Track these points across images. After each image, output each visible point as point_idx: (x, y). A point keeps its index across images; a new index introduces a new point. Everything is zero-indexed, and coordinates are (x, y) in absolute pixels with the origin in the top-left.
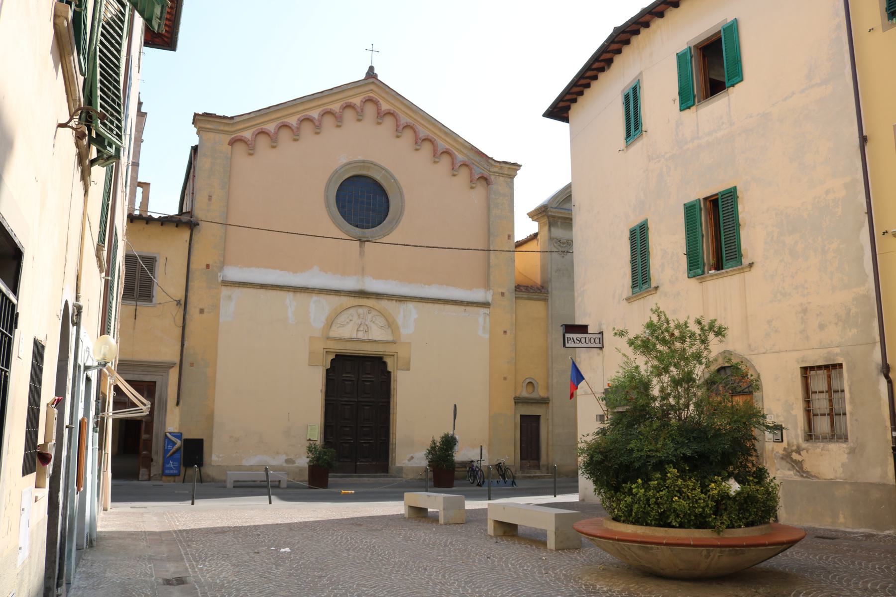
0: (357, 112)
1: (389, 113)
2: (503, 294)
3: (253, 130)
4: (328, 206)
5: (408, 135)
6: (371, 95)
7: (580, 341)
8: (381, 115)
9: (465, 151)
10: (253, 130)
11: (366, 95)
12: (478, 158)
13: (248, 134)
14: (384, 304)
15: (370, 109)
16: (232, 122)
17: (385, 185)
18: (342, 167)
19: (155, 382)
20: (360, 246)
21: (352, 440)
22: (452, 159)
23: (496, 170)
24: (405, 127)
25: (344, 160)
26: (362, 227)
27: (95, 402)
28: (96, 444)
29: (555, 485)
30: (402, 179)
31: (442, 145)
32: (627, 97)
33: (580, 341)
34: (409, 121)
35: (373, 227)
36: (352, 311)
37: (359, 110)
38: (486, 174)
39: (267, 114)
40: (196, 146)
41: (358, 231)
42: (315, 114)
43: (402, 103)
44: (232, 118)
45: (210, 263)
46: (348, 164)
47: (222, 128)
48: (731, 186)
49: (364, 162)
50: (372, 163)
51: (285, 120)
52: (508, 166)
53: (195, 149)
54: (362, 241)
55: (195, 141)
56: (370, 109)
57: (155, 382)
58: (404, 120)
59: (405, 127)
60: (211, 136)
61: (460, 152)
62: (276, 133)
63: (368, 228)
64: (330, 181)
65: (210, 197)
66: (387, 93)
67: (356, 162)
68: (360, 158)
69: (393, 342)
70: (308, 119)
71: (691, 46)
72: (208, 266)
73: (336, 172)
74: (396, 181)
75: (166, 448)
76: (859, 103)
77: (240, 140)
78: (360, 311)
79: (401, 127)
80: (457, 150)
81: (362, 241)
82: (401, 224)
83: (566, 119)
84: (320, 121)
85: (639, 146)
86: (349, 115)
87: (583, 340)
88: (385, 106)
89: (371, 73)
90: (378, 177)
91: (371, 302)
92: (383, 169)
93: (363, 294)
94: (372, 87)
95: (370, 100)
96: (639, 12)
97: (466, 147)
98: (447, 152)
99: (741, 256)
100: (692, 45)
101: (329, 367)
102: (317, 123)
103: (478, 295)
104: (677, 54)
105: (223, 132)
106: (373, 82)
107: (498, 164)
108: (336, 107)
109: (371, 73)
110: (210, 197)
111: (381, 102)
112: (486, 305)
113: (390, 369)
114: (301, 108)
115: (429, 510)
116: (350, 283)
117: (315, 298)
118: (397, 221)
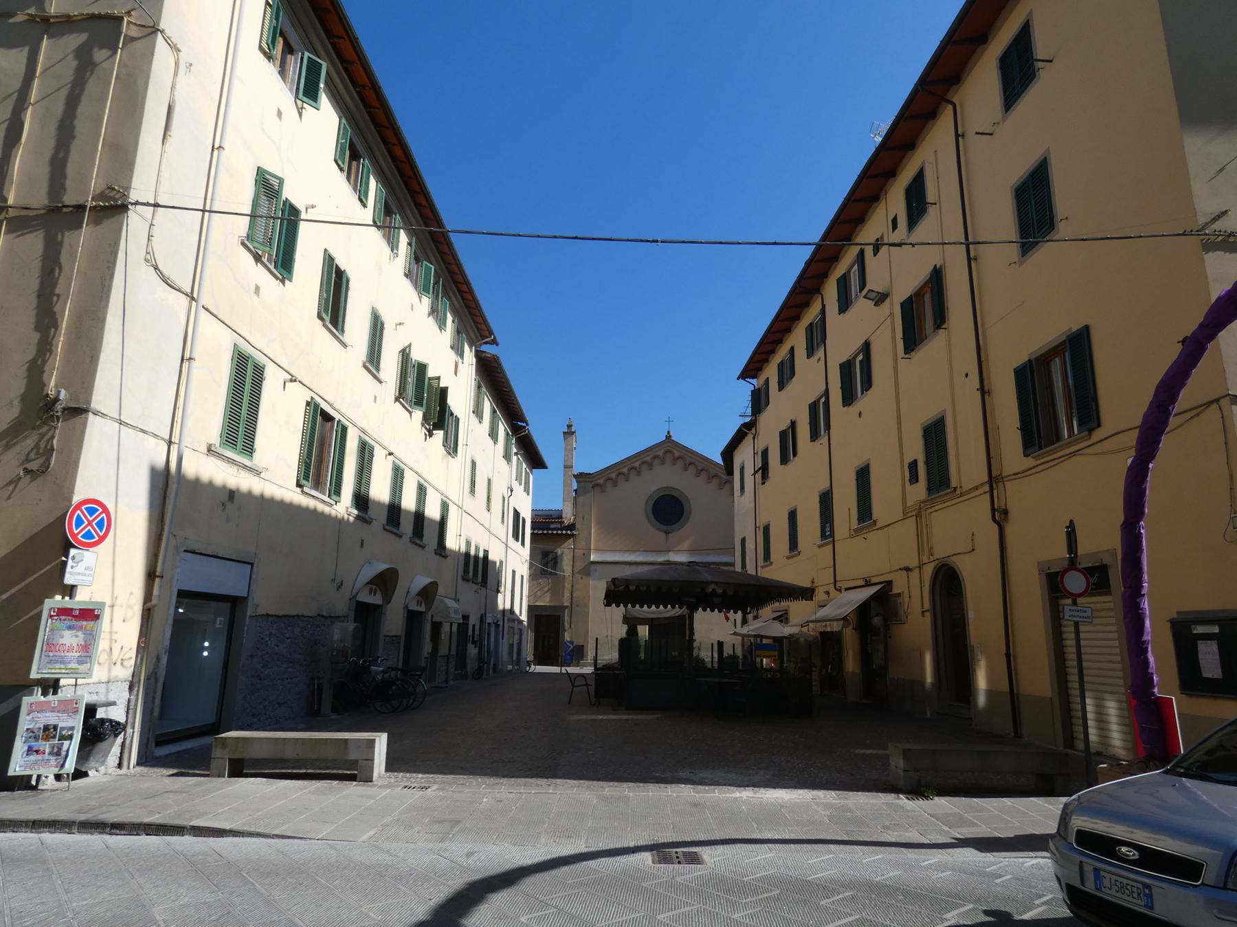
1: (680, 457)
3: (604, 478)
4: (650, 522)
6: (668, 448)
8: (675, 460)
10: (604, 478)
11: (617, 472)
13: (601, 481)
15: (668, 456)
17: (680, 498)
19: (559, 616)
21: (303, 54)
25: (654, 488)
29: (387, 227)
34: (691, 460)
41: (665, 528)
46: (658, 490)
47: (587, 480)
50: (671, 488)
51: (620, 471)
54: (667, 533)
56: (668, 456)
57: (559, 616)
58: (689, 460)
60: (582, 484)
62: (628, 474)
65: (583, 518)
68: (664, 486)
71: (1031, 359)
73: (651, 495)
76: (976, 313)
77: (598, 485)
81: (667, 533)
84: (640, 468)
88: (677, 454)
89: (668, 437)
90: (675, 494)
94: (669, 444)
95: (668, 452)
100: (1033, 357)
104: (1014, 369)
108: (648, 459)
109: (668, 437)
110: (583, 518)
111: (675, 451)
114: (629, 463)
115: (575, 488)
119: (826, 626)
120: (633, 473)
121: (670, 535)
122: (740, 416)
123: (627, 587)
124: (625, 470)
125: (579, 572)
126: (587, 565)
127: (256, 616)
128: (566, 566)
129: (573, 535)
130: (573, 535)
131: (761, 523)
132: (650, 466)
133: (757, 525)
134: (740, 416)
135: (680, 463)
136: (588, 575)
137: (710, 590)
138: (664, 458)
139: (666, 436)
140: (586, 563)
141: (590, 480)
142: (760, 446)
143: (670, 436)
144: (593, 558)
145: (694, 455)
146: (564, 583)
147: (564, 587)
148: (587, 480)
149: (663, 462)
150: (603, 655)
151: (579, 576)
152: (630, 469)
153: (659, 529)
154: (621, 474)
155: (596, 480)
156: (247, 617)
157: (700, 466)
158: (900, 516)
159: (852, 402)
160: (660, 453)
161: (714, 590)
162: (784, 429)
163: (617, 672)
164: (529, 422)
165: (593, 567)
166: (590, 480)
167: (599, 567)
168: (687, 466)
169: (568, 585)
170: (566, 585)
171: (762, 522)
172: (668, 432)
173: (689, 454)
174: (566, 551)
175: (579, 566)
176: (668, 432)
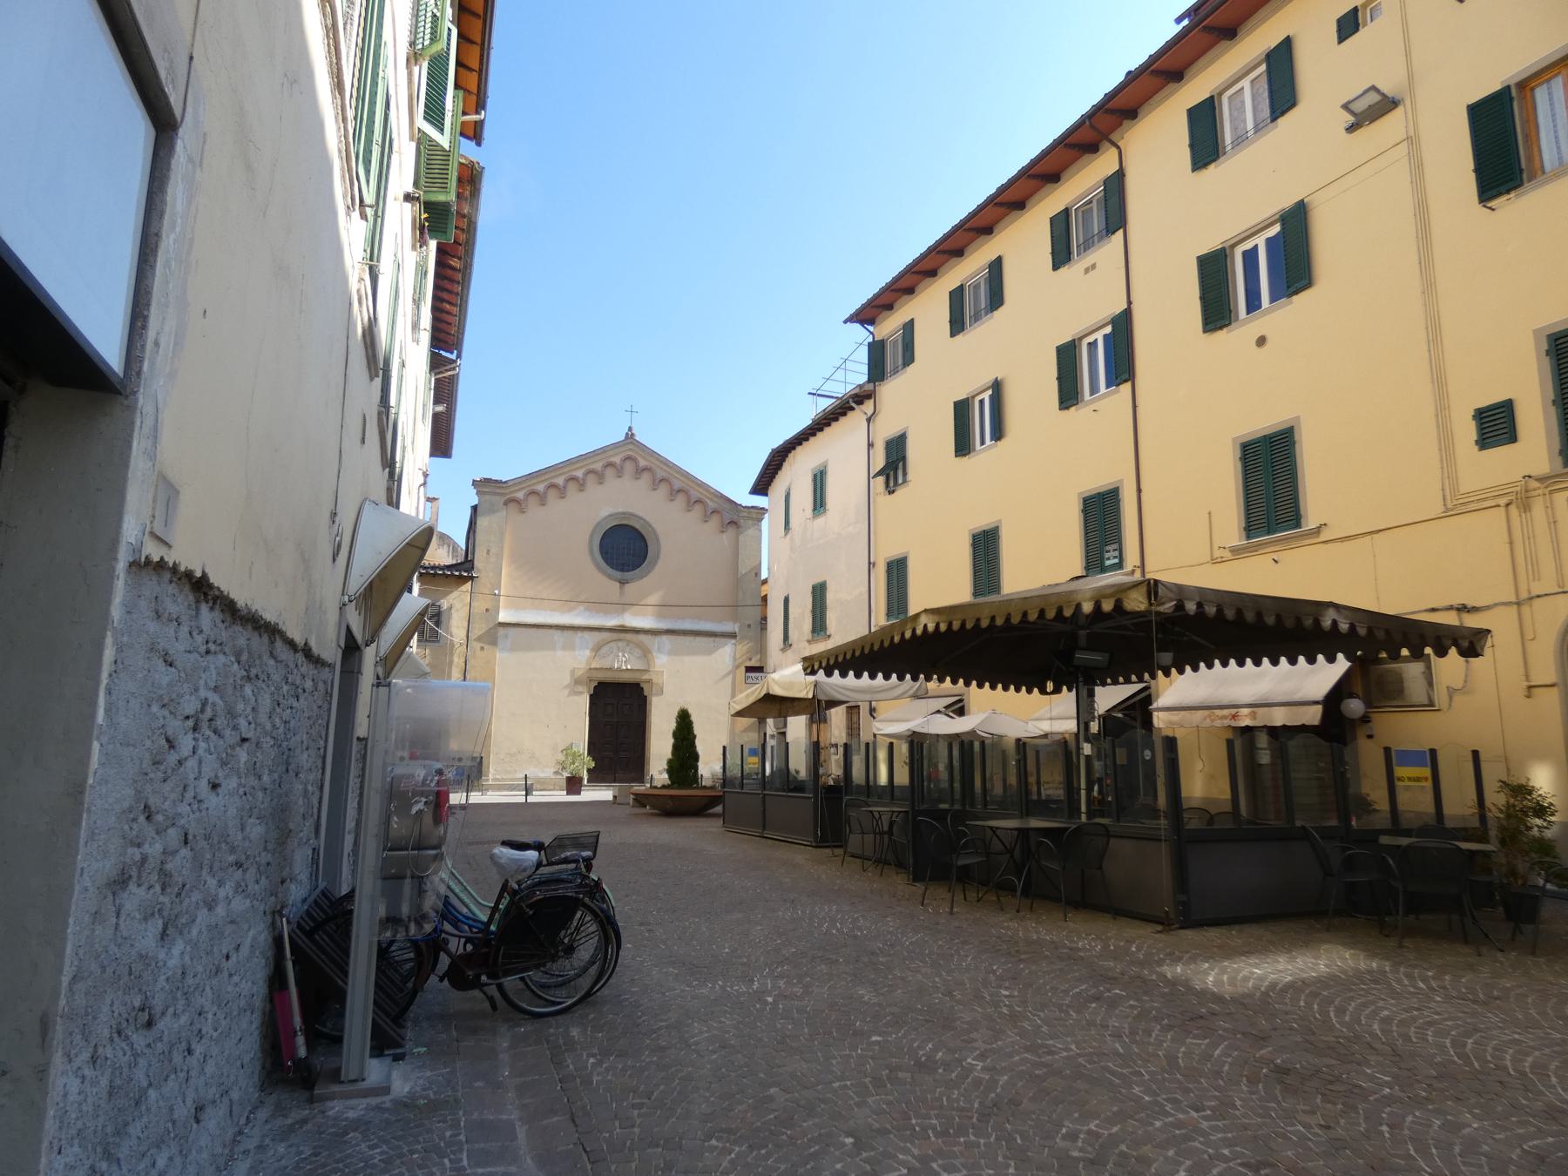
0: (618, 470)
1: (646, 469)
2: (749, 626)
5: (663, 489)
7: (757, 679)
8: (639, 471)
9: (715, 499)
11: (625, 454)
12: (727, 506)
13: (520, 495)
14: (642, 637)
15: (629, 466)
16: (504, 485)
18: (604, 519)
20: (621, 588)
22: (705, 507)
23: (745, 514)
24: (661, 481)
25: (605, 512)
26: (622, 570)
27: (391, 405)
28: (523, 855)
30: (659, 527)
31: (695, 495)
32: (815, 476)
33: (757, 679)
35: (633, 570)
36: (613, 644)
37: (619, 467)
38: (735, 518)
39: (537, 476)
40: (476, 505)
41: (618, 574)
42: (579, 474)
43: (658, 459)
44: (506, 482)
45: (490, 607)
46: (610, 516)
47: (498, 491)
48: (823, 580)
49: (624, 513)
52: (756, 511)
53: (475, 508)
54: (623, 583)
55: (475, 501)
56: (629, 466)
58: (660, 474)
59: (661, 481)
61: (711, 500)
62: (545, 493)
63: (628, 571)
64: (592, 536)
65: (488, 551)
66: (643, 451)
67: (616, 514)
68: (621, 510)
69: (646, 671)
70: (573, 479)
72: (487, 610)
73: (599, 523)
74: (653, 529)
75: (916, 808)
78: (620, 644)
79: (657, 481)
80: (707, 498)
81: (623, 583)
82: (657, 567)
83: (766, 495)
84: (545, 493)
85: (821, 520)
86: (610, 472)
87: (760, 678)
88: (642, 463)
89: (630, 436)
91: (629, 636)
92: (642, 519)
93: (623, 630)
94: (630, 446)
95: (629, 458)
96: (781, 443)
97: (716, 496)
98: (699, 501)
99: (826, 629)
101: (592, 693)
102: (581, 482)
103: (728, 627)
105: (499, 494)
106: (631, 443)
107: (745, 510)
108: (598, 466)
109: (630, 436)
110: (488, 551)
111: (639, 458)
112: (733, 636)
113: (645, 694)
116: (612, 622)
117: (580, 634)
118: (655, 563)
119: (1234, 717)
120: (552, 493)
121: (627, 585)
122: (810, 393)
123: (1180, 606)
124: (560, 481)
125: (479, 639)
126: (491, 629)
127: (161, 565)
128: (456, 629)
129: (472, 578)
130: (472, 578)
131: (882, 557)
132: (600, 477)
133: (872, 561)
134: (810, 393)
135: (646, 476)
136: (494, 643)
137: (1327, 623)
138: (622, 468)
139: (627, 434)
140: (491, 625)
141: (501, 491)
142: (886, 429)
143: (632, 434)
144: (503, 617)
145: (668, 466)
146: (452, 655)
147: (451, 663)
148: (498, 491)
149: (620, 473)
150: (516, 771)
151: (478, 645)
152: (567, 480)
153: (610, 577)
154: (553, 486)
155: (512, 492)
156: (121, 566)
157: (677, 485)
158: (1438, 509)
159: (1230, 324)
160: (617, 460)
161: (1335, 623)
162: (965, 397)
163: (1465, 846)
164: (464, 354)
165: (501, 631)
166: (501, 491)
167: (512, 631)
168: (656, 483)
169: (458, 661)
170: (456, 659)
171: (886, 551)
172: (630, 429)
173: (662, 466)
174: (457, 605)
175: (479, 629)
176: (630, 429)
